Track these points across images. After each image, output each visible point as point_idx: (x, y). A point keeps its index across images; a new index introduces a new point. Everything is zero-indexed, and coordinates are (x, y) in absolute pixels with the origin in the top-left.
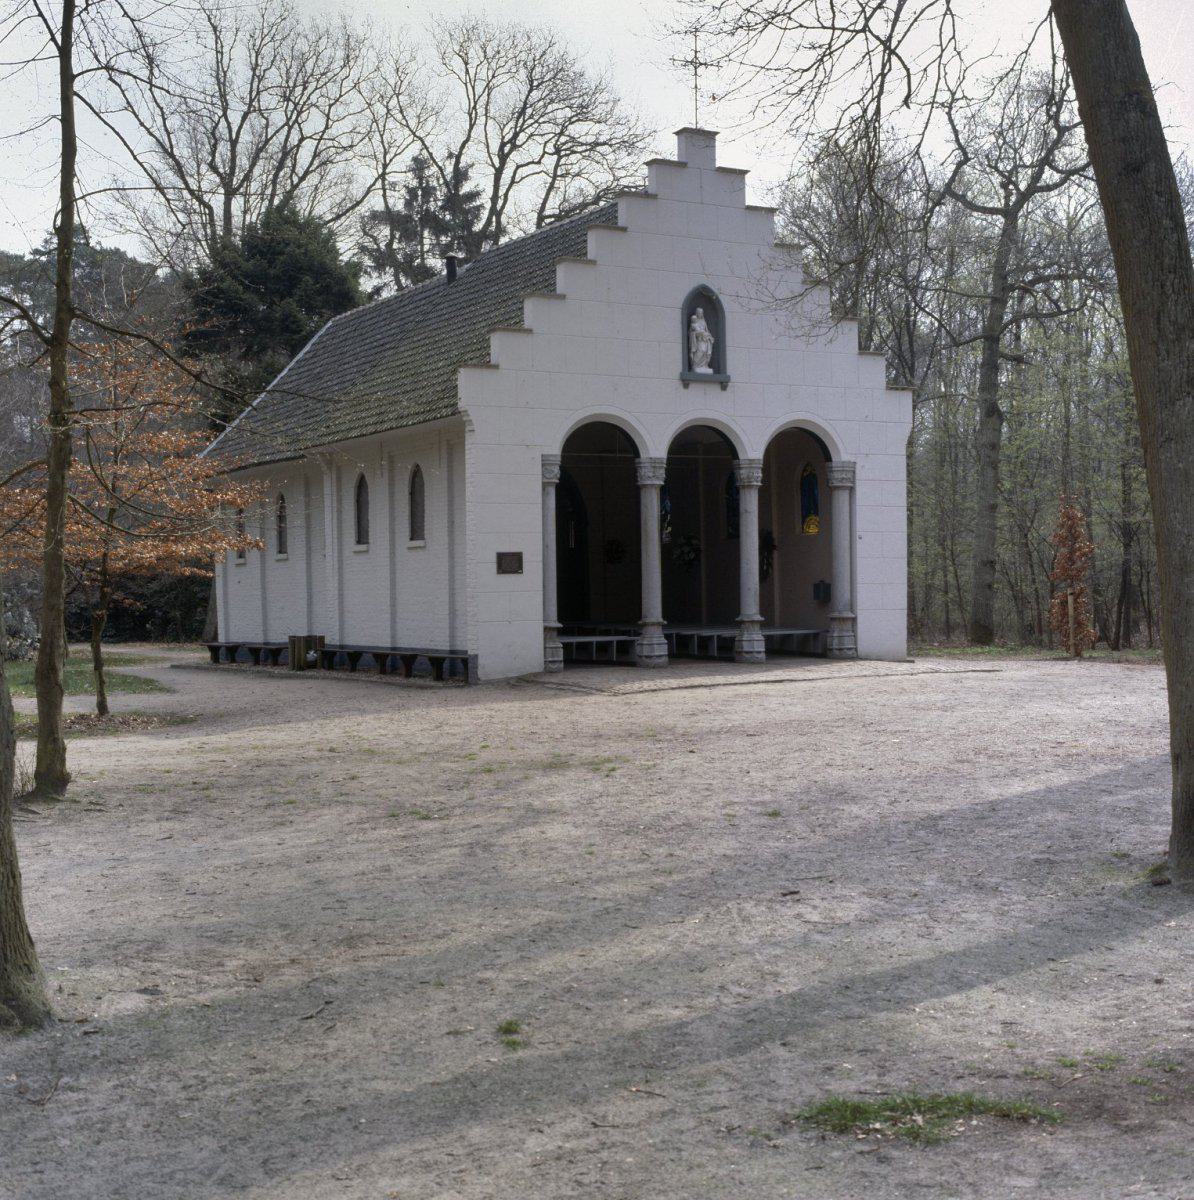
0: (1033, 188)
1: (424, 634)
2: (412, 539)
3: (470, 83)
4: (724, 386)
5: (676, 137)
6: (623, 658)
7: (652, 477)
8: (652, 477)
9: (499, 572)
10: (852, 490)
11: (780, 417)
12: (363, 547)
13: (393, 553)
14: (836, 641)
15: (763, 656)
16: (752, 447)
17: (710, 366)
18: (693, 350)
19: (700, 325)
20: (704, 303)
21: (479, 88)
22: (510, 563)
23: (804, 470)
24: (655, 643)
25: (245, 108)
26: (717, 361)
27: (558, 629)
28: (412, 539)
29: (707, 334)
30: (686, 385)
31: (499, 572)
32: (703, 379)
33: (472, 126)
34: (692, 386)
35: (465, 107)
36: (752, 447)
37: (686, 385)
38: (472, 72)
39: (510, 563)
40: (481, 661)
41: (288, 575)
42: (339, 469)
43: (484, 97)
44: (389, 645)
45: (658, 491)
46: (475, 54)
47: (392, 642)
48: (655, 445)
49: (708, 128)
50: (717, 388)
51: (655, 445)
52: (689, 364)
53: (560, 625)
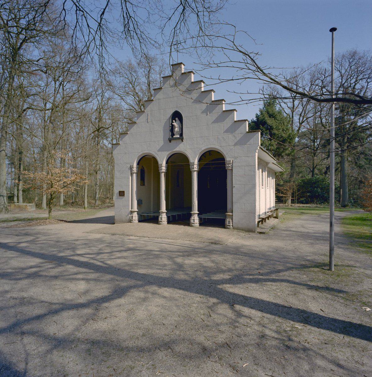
4: (182, 141)
10: (232, 170)
11: (204, 147)
24: (195, 219)
26: (181, 135)
34: (172, 141)
39: (122, 194)
50: (181, 140)
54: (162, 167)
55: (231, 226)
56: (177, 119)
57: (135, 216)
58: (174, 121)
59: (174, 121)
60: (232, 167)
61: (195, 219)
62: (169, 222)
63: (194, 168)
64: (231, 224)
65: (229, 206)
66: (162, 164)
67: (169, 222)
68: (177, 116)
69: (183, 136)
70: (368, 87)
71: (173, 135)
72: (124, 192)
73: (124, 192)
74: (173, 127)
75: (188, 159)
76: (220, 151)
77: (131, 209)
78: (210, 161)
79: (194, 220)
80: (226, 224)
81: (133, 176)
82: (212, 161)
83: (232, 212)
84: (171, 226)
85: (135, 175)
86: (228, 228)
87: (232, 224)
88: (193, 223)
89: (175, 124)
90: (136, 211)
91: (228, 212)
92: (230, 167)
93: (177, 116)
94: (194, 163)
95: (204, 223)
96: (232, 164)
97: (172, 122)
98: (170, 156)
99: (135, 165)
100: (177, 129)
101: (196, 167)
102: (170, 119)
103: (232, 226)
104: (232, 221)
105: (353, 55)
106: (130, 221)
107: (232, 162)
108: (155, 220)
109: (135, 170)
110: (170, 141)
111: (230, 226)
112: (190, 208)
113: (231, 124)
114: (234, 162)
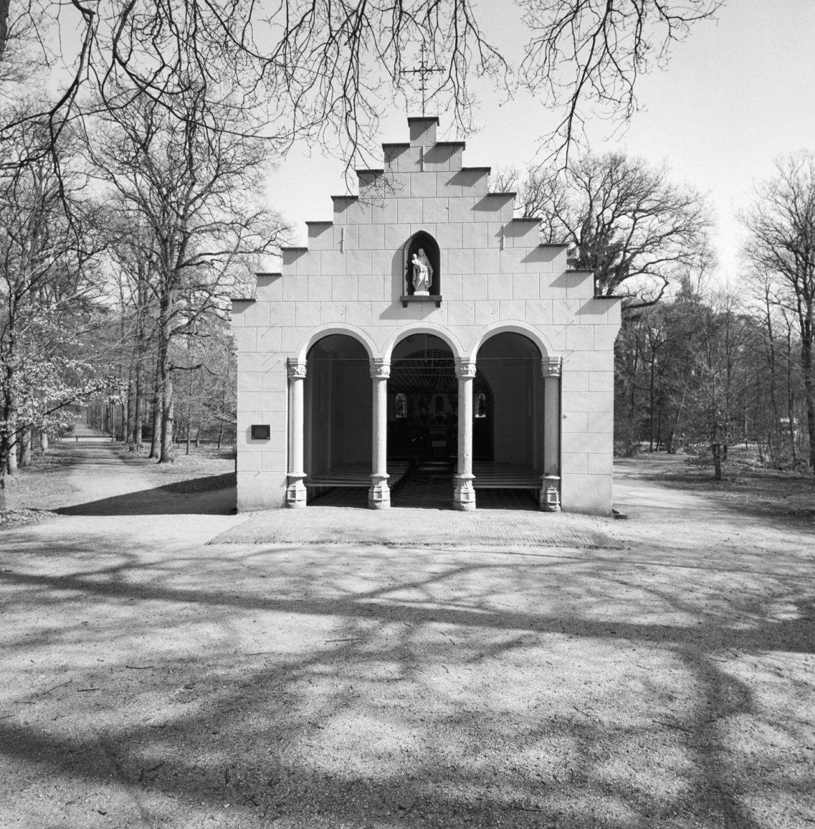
4: (438, 306)
10: (560, 379)
11: (493, 323)
16: (467, 352)
24: (467, 493)
26: (434, 288)
32: (421, 300)
34: (410, 305)
36: (467, 352)
39: (260, 433)
45: (385, 382)
48: (382, 352)
50: (433, 305)
51: (382, 352)
54: (382, 365)
55: (558, 506)
56: (421, 251)
57: (301, 490)
58: (415, 255)
59: (415, 255)
60: (561, 373)
61: (467, 493)
62: (481, 503)
63: (467, 371)
64: (558, 502)
65: (550, 460)
66: (382, 359)
67: (481, 503)
68: (423, 244)
69: (441, 294)
70: (636, 226)
71: (411, 289)
72: (267, 428)
73: (267, 428)
74: (411, 271)
75: (364, 348)
76: (435, 331)
77: (288, 472)
78: (406, 357)
79: (379, 493)
80: (546, 499)
81: (293, 385)
82: (406, 357)
83: (559, 474)
84: (393, 508)
85: (299, 386)
86: (551, 511)
87: (560, 500)
88: (465, 503)
89: (416, 261)
90: (299, 478)
91: (547, 475)
92: (553, 371)
93: (423, 244)
94: (381, 360)
95: (486, 499)
96: (561, 366)
97: (411, 258)
98: (321, 337)
99: (302, 360)
100: (424, 276)
101: (386, 371)
102: (403, 250)
103: (560, 505)
104: (560, 494)
105: (616, 162)
106: (287, 504)
107: (561, 362)
108: (361, 498)
109: (301, 371)
110: (405, 304)
111: (555, 504)
112: (367, 465)
113: (559, 275)
114: (564, 361)
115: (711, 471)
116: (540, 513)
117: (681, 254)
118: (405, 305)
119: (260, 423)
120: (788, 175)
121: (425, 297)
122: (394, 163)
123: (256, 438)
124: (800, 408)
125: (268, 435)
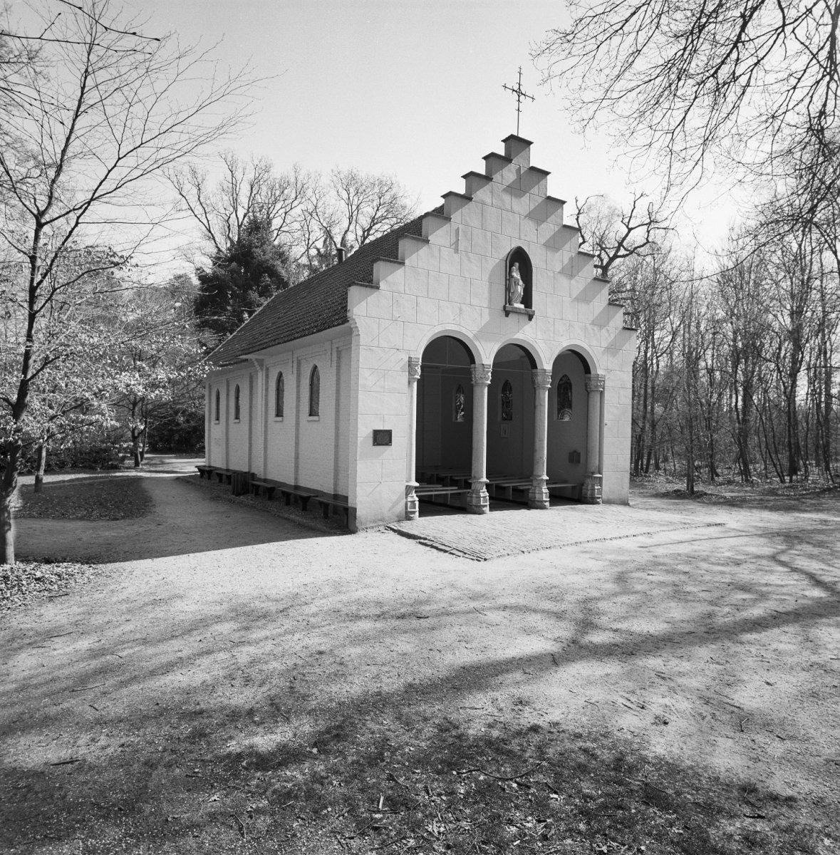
0: (616, 256)
1: (316, 479)
2: (310, 415)
3: (349, 204)
4: (530, 318)
5: (503, 144)
6: (461, 506)
7: (483, 380)
8: (483, 380)
9: (374, 445)
10: (602, 393)
11: (564, 343)
12: (280, 419)
13: (298, 424)
14: (589, 492)
15: (547, 504)
17: (522, 303)
18: (512, 291)
19: (516, 275)
20: (519, 258)
21: (354, 208)
22: (382, 438)
23: (561, 380)
25: (246, 211)
26: (527, 300)
27: (416, 488)
28: (310, 415)
29: (521, 283)
30: (507, 314)
31: (374, 445)
32: (517, 312)
33: (350, 223)
35: (348, 216)
37: (507, 315)
38: (351, 199)
40: (358, 513)
41: (239, 431)
42: (267, 369)
43: (356, 212)
44: (293, 483)
46: (352, 190)
47: (335, 490)
48: (486, 355)
49: (527, 138)
50: (527, 318)
51: (486, 355)
52: (509, 301)
53: (417, 484)
72: (389, 433)
73: (389, 433)
85: (415, 385)
86: (598, 503)
113: (601, 309)
115: (682, 486)
116: (469, 516)
117: (621, 32)
118: (507, 315)
119: (381, 428)
120: (680, 680)
121: (519, 309)
122: (559, 275)
123: (378, 444)
124: (606, 851)
125: (390, 441)
